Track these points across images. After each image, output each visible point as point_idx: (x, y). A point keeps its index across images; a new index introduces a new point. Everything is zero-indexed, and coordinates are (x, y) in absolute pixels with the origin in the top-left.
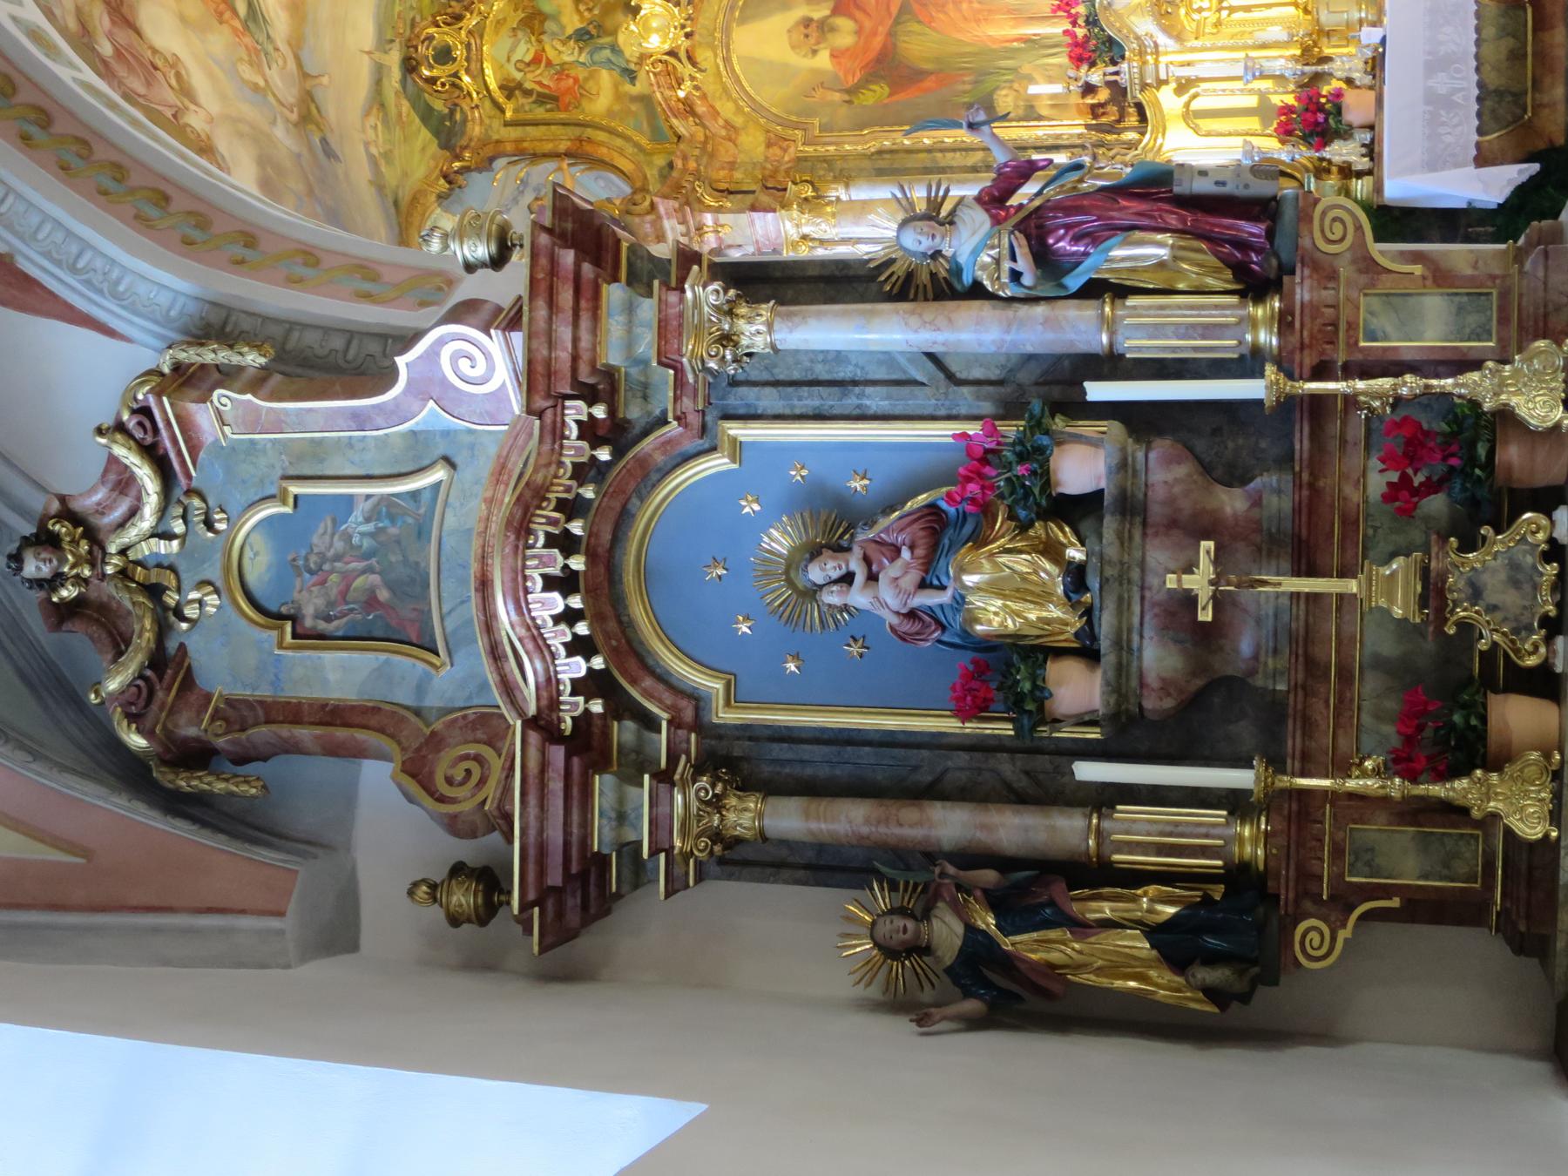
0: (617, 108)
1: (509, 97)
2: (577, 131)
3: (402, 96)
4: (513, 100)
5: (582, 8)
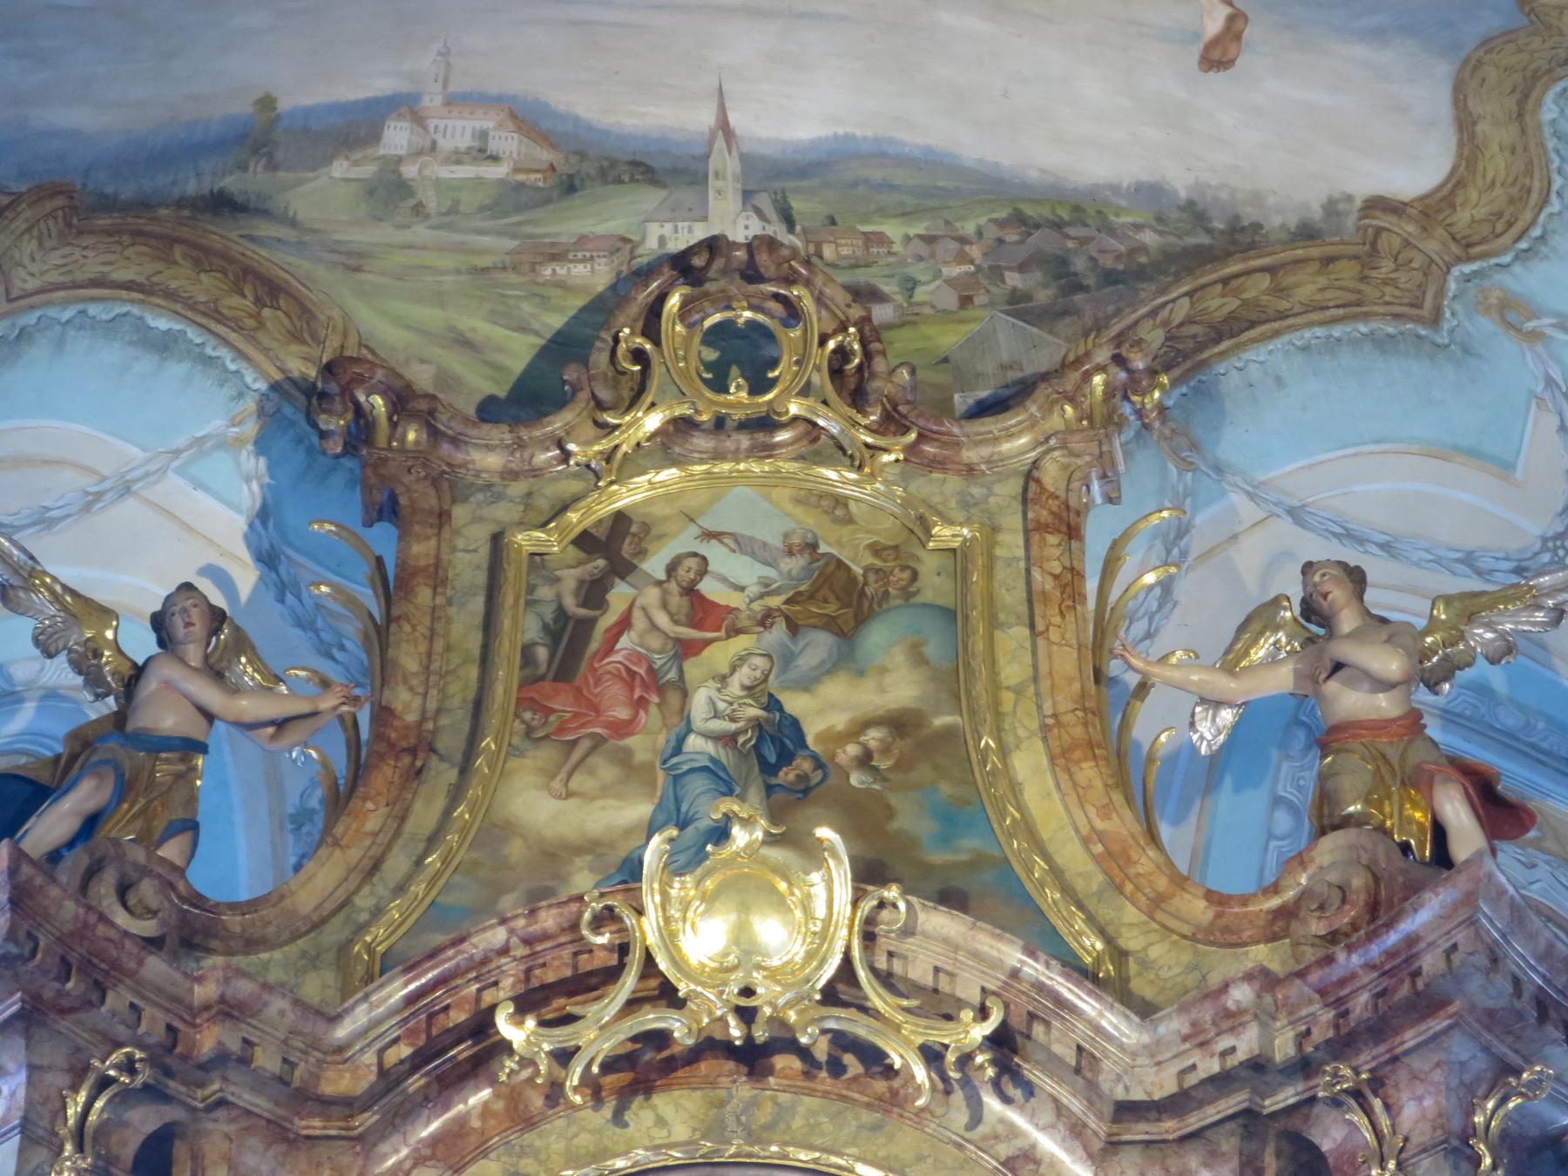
0: (515, 850)
1: (585, 541)
2: (451, 741)
3: (621, 263)
4: (574, 553)
5: (873, 737)
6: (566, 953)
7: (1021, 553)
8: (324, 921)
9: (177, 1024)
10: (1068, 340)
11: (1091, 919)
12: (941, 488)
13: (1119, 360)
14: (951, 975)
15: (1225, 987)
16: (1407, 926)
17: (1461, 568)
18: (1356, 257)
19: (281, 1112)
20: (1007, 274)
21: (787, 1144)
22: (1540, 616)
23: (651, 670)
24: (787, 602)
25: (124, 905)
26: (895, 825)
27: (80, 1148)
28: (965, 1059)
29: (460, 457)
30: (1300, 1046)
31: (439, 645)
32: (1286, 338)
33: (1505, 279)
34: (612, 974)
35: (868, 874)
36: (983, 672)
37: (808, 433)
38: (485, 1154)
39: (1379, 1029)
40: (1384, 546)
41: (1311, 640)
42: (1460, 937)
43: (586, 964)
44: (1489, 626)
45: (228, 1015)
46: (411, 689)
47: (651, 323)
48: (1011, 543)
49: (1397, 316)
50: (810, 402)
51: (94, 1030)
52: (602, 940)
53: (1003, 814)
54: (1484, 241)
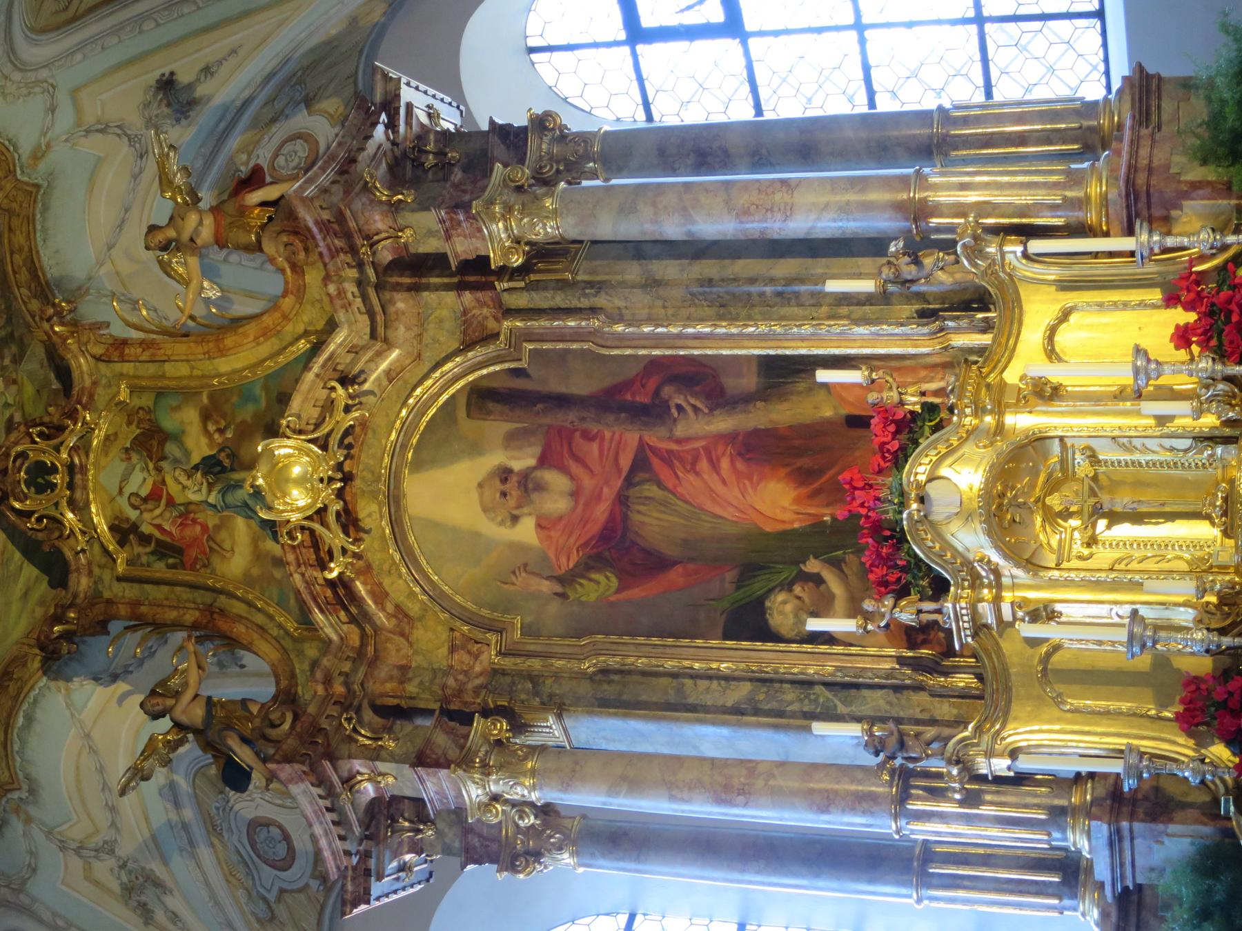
1: (122, 543)
2: (208, 598)
4: (127, 548)
6: (304, 550)
7: (132, 364)
8: (283, 648)
9: (332, 701)
10: (32, 339)
11: (291, 344)
12: (102, 395)
13: (48, 320)
14: (316, 400)
15: (329, 295)
16: (311, 224)
17: (138, 180)
18: (10, 218)
19: (365, 663)
20: (5, 364)
21: (381, 467)
22: (172, 154)
23: (180, 517)
24: (151, 460)
25: (279, 725)
26: (249, 420)
27: (380, 739)
28: (351, 397)
29: (82, 595)
30: (353, 267)
31: (165, 603)
32: (40, 249)
33: (24, 157)
34: (312, 532)
35: (273, 431)
36: (185, 382)
37: (76, 451)
38: (381, 584)
39: (348, 236)
40: (127, 211)
41: (178, 250)
42: (317, 204)
43: (308, 542)
44: (175, 175)
45: (330, 681)
46: (185, 614)
47: (26, 515)
48: (128, 368)
49: (35, 202)
50: (62, 449)
51: (335, 733)
52: (299, 535)
53: (247, 377)
54: (8, 165)
